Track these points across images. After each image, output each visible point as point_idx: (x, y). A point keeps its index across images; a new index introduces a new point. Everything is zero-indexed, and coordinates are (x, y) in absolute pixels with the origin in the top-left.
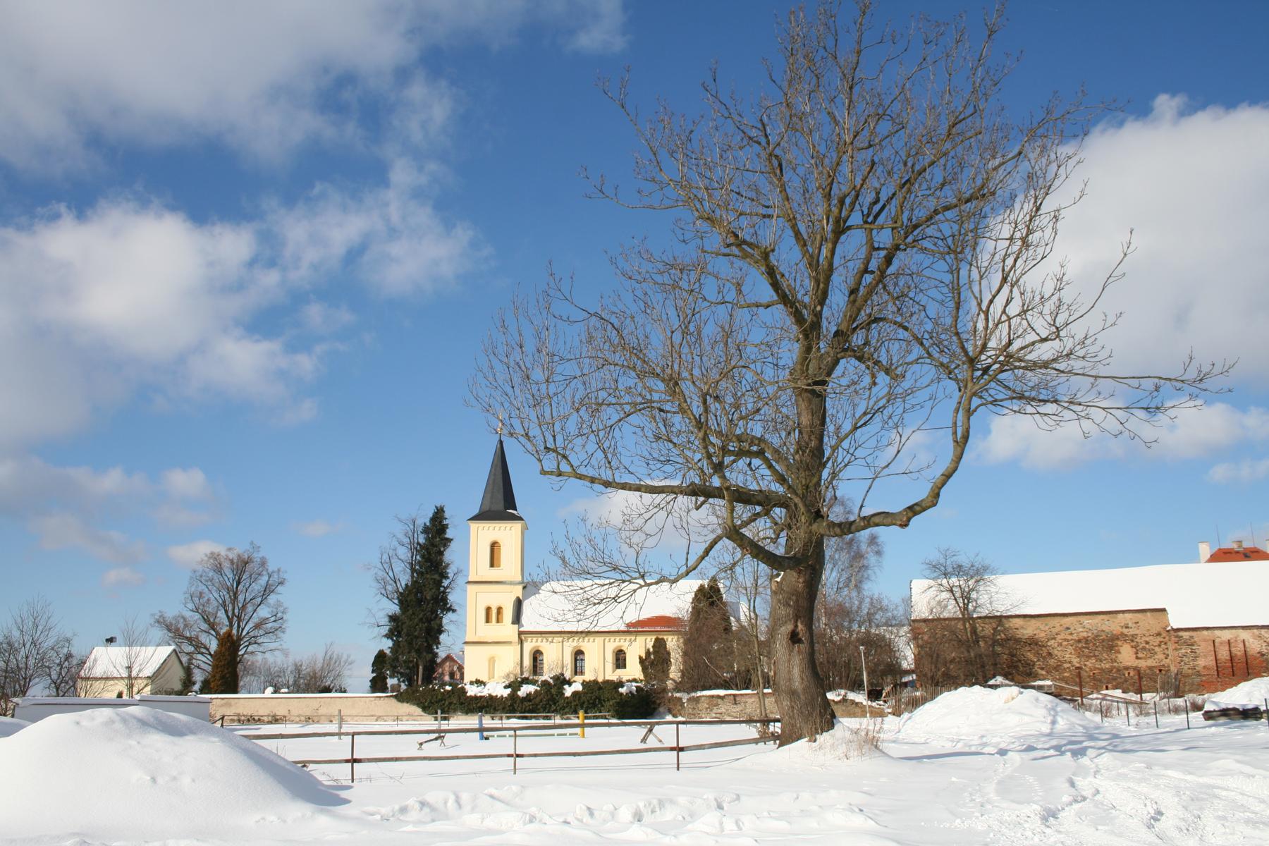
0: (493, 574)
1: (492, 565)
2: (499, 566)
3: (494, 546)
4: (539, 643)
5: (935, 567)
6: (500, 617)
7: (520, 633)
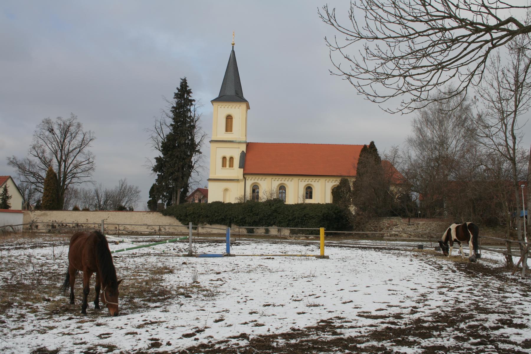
2: (231, 131)
3: (229, 118)
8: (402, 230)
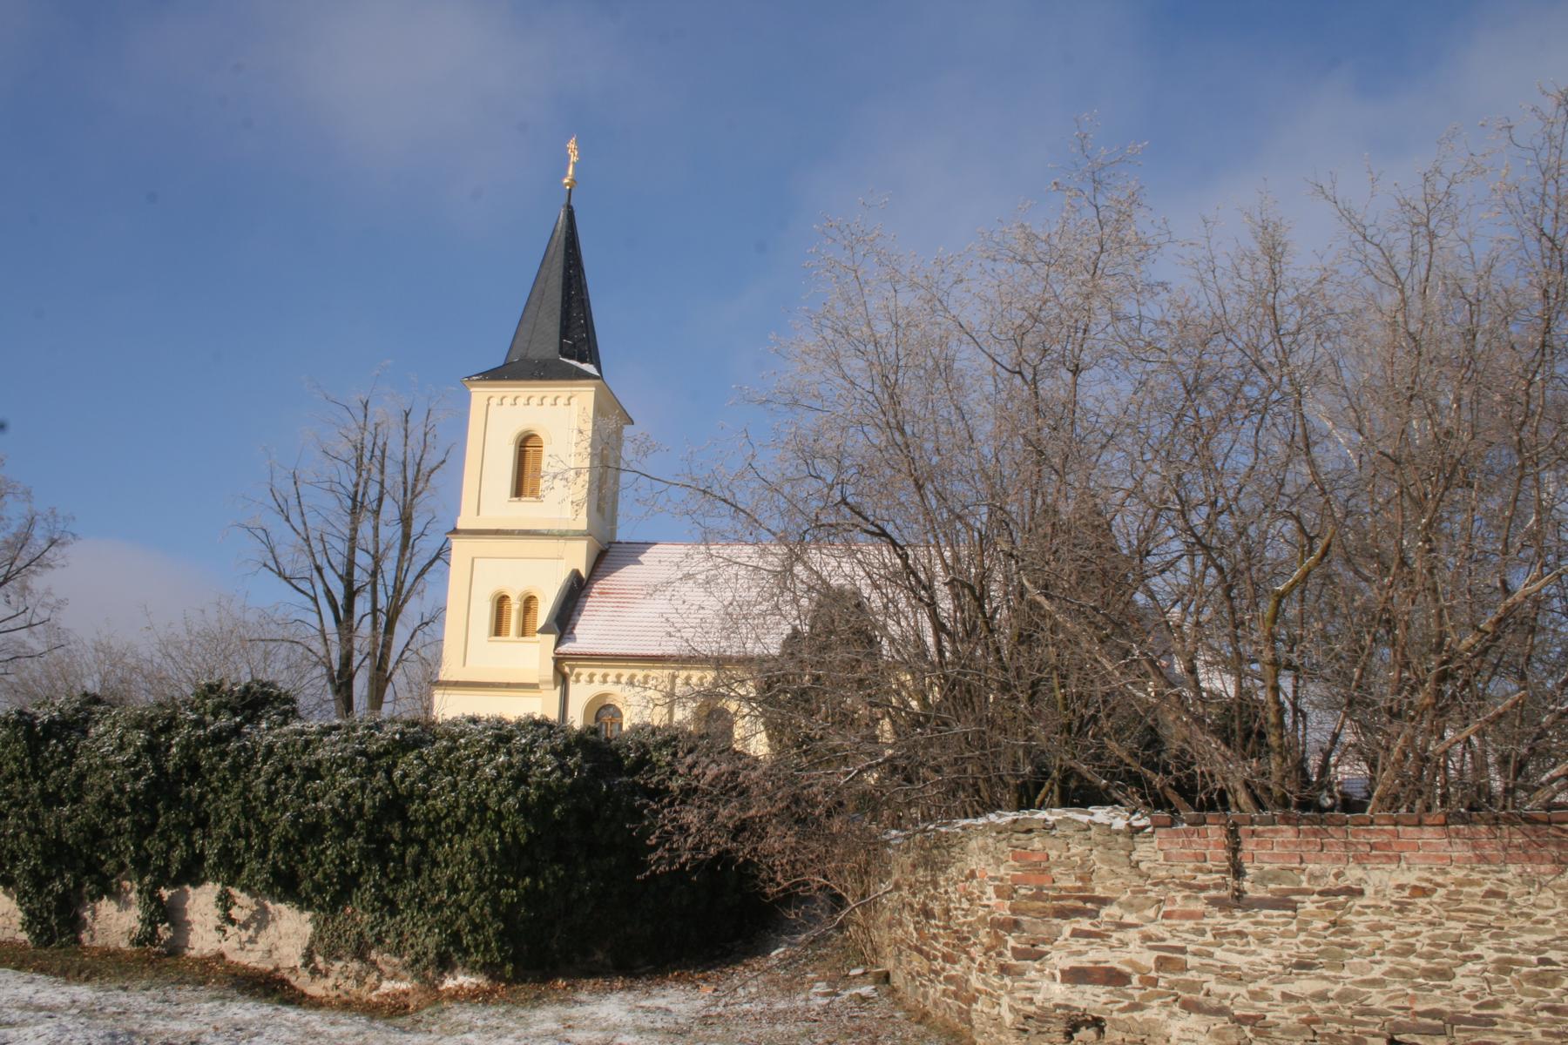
0: (524, 513)
1: (518, 491)
2: (534, 493)
3: (526, 446)
4: (608, 688)
5: (347, 711)
6: (529, 617)
7: (559, 661)
8: (1148, 959)
